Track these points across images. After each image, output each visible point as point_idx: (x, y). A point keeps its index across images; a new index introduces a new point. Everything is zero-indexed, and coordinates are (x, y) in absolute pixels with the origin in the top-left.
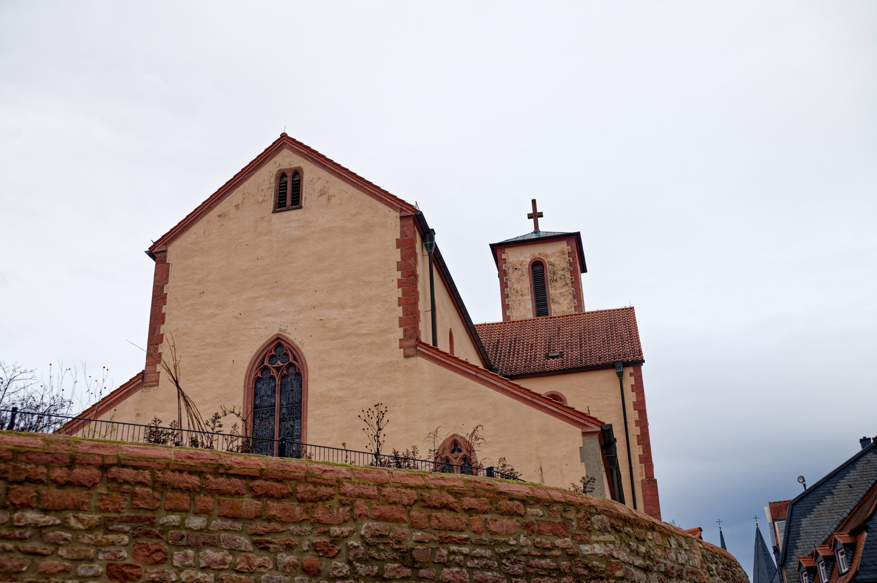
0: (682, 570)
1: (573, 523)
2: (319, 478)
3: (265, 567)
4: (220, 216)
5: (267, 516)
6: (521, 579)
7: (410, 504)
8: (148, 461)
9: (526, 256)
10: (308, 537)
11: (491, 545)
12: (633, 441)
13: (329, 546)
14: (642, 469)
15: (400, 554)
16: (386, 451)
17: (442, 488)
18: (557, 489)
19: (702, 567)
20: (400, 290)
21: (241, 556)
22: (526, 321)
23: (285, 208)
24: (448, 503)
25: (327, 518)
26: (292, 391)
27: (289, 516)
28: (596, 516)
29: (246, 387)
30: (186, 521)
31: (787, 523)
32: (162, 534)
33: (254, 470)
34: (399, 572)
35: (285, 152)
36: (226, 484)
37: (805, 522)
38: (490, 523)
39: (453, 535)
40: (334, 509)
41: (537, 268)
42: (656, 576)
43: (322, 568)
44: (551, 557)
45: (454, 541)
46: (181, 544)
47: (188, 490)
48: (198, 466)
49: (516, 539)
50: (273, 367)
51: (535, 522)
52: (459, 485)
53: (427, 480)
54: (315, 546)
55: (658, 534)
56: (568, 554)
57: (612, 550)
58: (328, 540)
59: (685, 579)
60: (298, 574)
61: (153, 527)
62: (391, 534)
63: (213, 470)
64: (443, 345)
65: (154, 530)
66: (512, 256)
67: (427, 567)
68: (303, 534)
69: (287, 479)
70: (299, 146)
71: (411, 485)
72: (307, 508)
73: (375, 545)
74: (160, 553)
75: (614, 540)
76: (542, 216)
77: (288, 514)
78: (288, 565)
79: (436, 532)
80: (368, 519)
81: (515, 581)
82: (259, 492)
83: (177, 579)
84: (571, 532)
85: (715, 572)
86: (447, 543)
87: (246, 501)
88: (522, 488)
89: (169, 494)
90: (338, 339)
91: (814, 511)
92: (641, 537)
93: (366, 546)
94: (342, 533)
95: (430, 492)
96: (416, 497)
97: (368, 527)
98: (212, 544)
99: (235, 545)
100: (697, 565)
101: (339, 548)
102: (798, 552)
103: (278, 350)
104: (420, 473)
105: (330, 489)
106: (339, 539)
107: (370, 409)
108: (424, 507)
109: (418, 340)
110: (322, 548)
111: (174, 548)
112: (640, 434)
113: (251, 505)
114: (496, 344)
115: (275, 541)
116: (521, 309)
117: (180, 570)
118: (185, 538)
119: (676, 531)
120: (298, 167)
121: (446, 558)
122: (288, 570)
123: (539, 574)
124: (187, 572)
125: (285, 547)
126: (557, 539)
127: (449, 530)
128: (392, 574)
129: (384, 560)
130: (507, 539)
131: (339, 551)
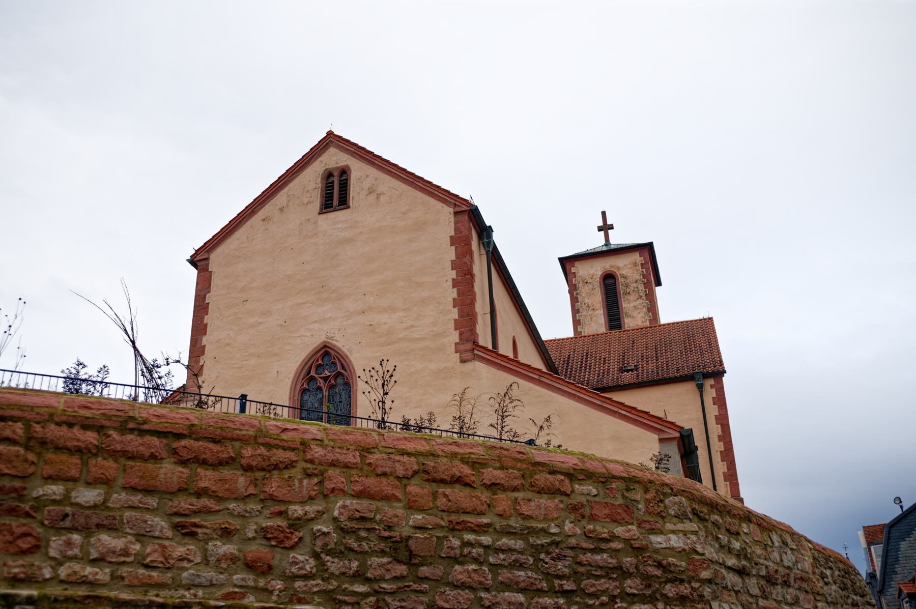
0: (788, 574)
1: (640, 506)
2: (275, 439)
3: (189, 561)
4: (263, 220)
5: (196, 489)
6: (567, 581)
7: (406, 476)
8: (23, 410)
9: (596, 269)
10: (255, 520)
11: (522, 534)
12: (717, 458)
13: (286, 532)
14: (727, 487)
15: (391, 545)
16: (394, 417)
17: (454, 456)
18: (617, 462)
19: (814, 573)
20: (455, 290)
21: (153, 543)
22: (598, 335)
23: (332, 209)
24: (462, 475)
25: (285, 494)
26: (341, 402)
27: (228, 490)
28: (671, 498)
29: (292, 400)
30: (73, 494)
31: (884, 547)
32: (35, 512)
33: (181, 426)
34: (389, 570)
35: (332, 150)
36: (137, 443)
37: (903, 545)
38: (522, 503)
39: (469, 519)
40: (296, 480)
41: (609, 281)
42: (756, 582)
43: (275, 563)
44: (609, 551)
45: (470, 527)
46: (63, 526)
47: (83, 452)
48: (97, 419)
49: (559, 526)
50: (320, 377)
51: (585, 503)
52: (478, 452)
53: (433, 445)
54: (265, 531)
55: (756, 527)
56: (632, 548)
57: (695, 543)
58: (285, 523)
59: (793, 587)
60: (238, 571)
61: (22, 501)
62: (378, 517)
63: (119, 424)
64: (505, 349)
65: (22, 505)
66: (582, 270)
67: (431, 563)
68: (248, 515)
69: (229, 439)
70: (346, 143)
71: (409, 450)
72: (256, 479)
73: (353, 531)
74: (29, 539)
75: (697, 530)
76: (613, 228)
77: (227, 486)
78: (224, 558)
79: (444, 514)
80: (345, 496)
81: (559, 584)
82: (186, 455)
83: (53, 575)
84: (637, 518)
85: (830, 580)
86: (460, 531)
87: (166, 468)
88: (568, 458)
89: (50, 455)
90: (388, 345)
91: (912, 534)
92: (734, 529)
93: (341, 533)
94: (306, 514)
95: (436, 461)
96: (416, 467)
97: (344, 507)
98: (110, 527)
99: (145, 528)
100: (807, 570)
101: (301, 534)
102: (898, 578)
103: (326, 359)
104: (425, 437)
105: (290, 453)
106: (301, 522)
107: (373, 368)
108: (427, 480)
109: (476, 343)
110: (275, 535)
111: (52, 532)
112: (723, 450)
113: (173, 473)
114: (566, 359)
115: (205, 524)
116: (593, 324)
117: (58, 563)
118: (70, 518)
119: (778, 526)
120: (345, 166)
121: (458, 552)
122: (224, 566)
123: (593, 575)
124: (70, 567)
125: (220, 533)
126: (617, 527)
127: (462, 513)
128: (379, 572)
129: (366, 553)
130: (546, 525)
131: (301, 539)
